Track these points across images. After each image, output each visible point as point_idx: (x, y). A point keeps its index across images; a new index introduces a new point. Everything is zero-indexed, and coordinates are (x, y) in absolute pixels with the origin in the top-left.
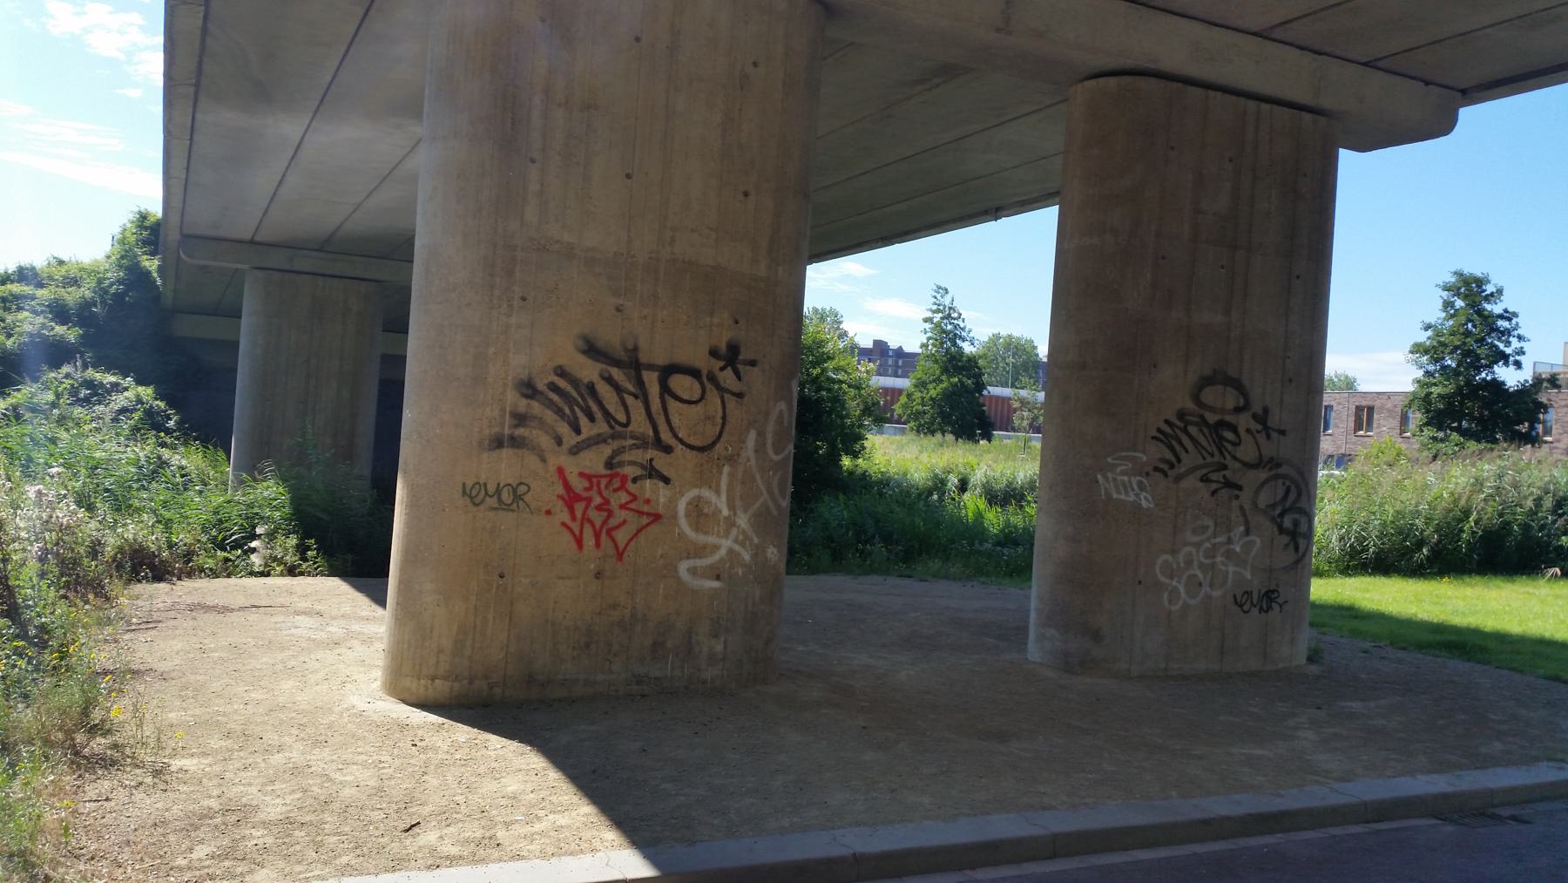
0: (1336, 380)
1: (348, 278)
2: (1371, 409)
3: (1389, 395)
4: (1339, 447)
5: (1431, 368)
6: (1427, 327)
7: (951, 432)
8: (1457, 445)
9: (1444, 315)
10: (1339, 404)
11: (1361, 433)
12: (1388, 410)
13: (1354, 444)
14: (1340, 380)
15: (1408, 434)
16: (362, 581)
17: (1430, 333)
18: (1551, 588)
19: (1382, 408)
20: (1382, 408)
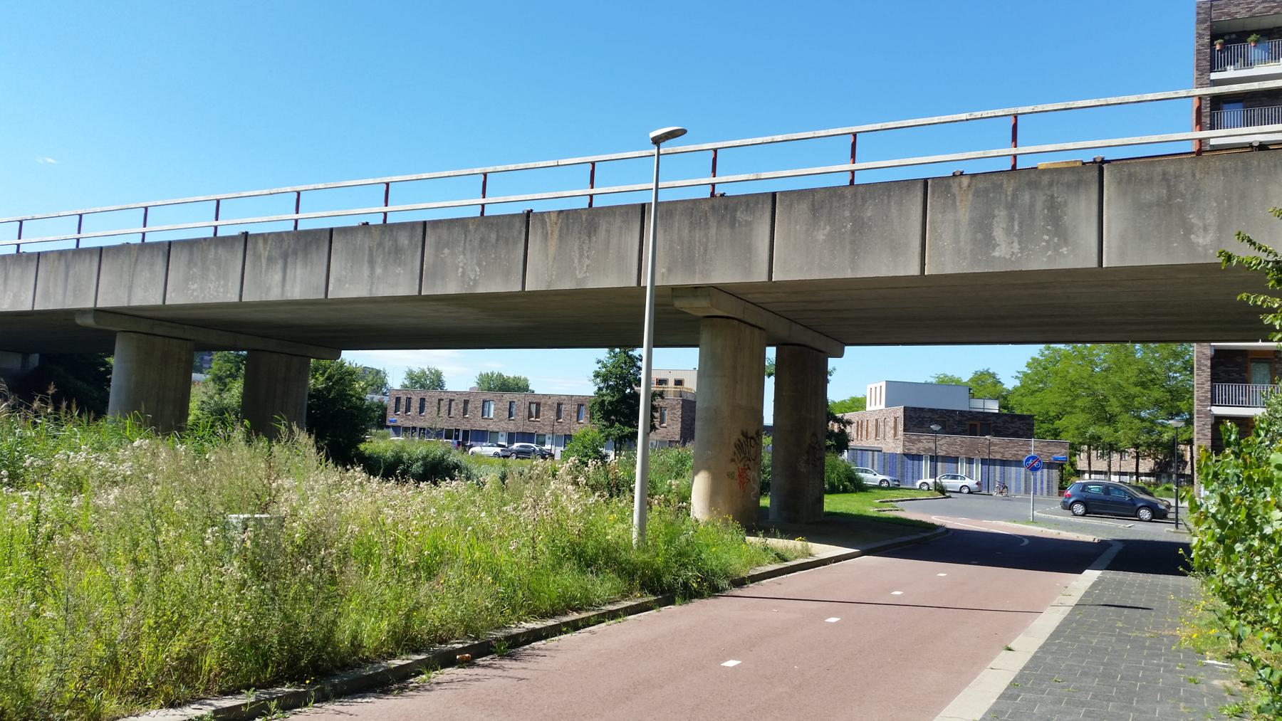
0: (427, 373)
1: (818, 332)
2: (538, 405)
3: (550, 396)
4: (518, 428)
5: (602, 385)
6: (599, 362)
7: (1156, 463)
8: (619, 430)
9: (609, 355)
10: (519, 400)
11: (532, 419)
12: (549, 405)
13: (528, 426)
14: (431, 372)
15: (664, 425)
16: (1090, 565)
17: (600, 365)
18: (865, 512)
19: (545, 404)
20: (545, 404)
